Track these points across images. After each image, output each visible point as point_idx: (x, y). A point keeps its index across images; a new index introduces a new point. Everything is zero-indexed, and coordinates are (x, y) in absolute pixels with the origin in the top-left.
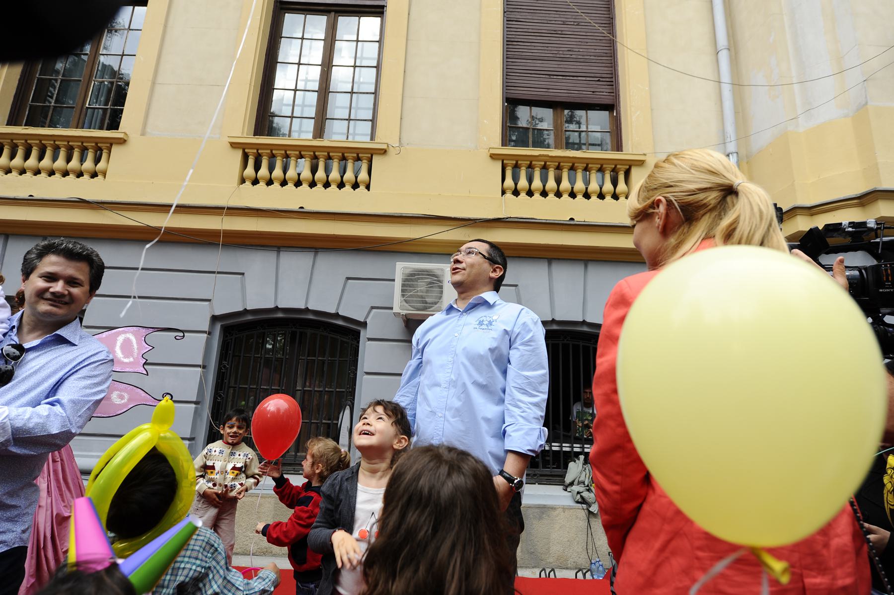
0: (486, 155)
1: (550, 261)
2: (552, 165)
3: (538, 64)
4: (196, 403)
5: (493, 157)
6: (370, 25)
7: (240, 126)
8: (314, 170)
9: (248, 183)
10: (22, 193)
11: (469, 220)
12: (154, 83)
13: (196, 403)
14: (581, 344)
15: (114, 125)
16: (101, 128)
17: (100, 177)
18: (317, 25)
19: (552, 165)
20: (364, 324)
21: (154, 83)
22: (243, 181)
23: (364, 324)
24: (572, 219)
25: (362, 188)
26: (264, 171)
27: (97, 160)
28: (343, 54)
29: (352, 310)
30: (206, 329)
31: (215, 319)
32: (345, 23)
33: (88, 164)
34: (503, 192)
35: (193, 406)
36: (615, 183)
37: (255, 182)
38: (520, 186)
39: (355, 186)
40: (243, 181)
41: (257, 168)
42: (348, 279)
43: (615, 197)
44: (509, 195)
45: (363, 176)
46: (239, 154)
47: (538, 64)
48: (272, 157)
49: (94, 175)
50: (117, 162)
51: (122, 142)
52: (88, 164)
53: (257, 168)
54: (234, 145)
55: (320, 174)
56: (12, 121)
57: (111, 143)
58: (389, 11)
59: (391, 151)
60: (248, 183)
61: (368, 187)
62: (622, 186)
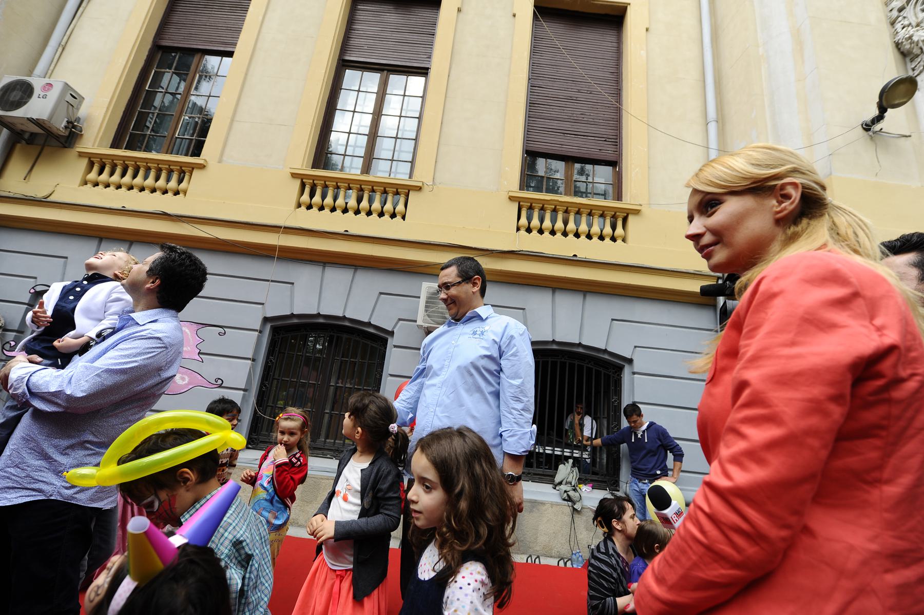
0: (505, 197)
1: (554, 290)
2: (561, 209)
3: (555, 124)
4: (244, 390)
5: (512, 199)
6: (416, 83)
7: (300, 157)
8: (359, 200)
9: (303, 208)
10: (569, 254)
11: (487, 250)
12: (232, 120)
13: (244, 390)
14: (576, 363)
15: (197, 151)
16: (186, 155)
17: (181, 195)
18: (372, 80)
19: (561, 209)
20: (391, 333)
21: (232, 120)
22: (299, 206)
23: (391, 333)
24: (575, 256)
25: (399, 218)
26: (317, 199)
27: (180, 181)
28: (393, 105)
29: (382, 320)
30: (258, 328)
31: (266, 320)
32: (396, 81)
33: (173, 184)
34: (518, 229)
35: (242, 392)
36: (614, 228)
37: (309, 207)
38: (532, 224)
39: (393, 216)
40: (299, 206)
41: (312, 195)
42: (381, 293)
43: (613, 239)
44: (523, 232)
45: (400, 207)
46: (298, 183)
47: (555, 124)
48: (326, 187)
49: (177, 193)
50: (196, 183)
51: (202, 167)
52: (173, 184)
53: (312, 195)
54: (294, 175)
55: (365, 204)
56: (115, 145)
57: (193, 167)
58: (432, 73)
59: (425, 188)
60: (303, 208)
61: (404, 218)
62: (619, 231)
